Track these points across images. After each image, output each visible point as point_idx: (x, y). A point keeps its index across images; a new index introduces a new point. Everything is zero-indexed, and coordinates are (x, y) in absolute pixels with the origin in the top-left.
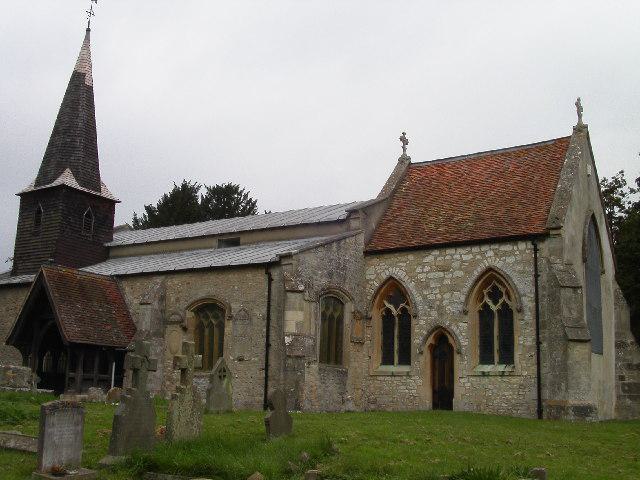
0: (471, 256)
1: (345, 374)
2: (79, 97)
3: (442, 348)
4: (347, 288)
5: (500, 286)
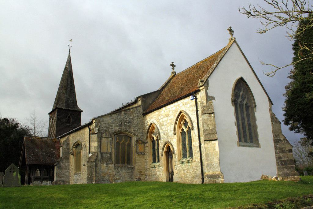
1: (134, 168)
2: (68, 75)
3: (169, 153)
4: (132, 130)
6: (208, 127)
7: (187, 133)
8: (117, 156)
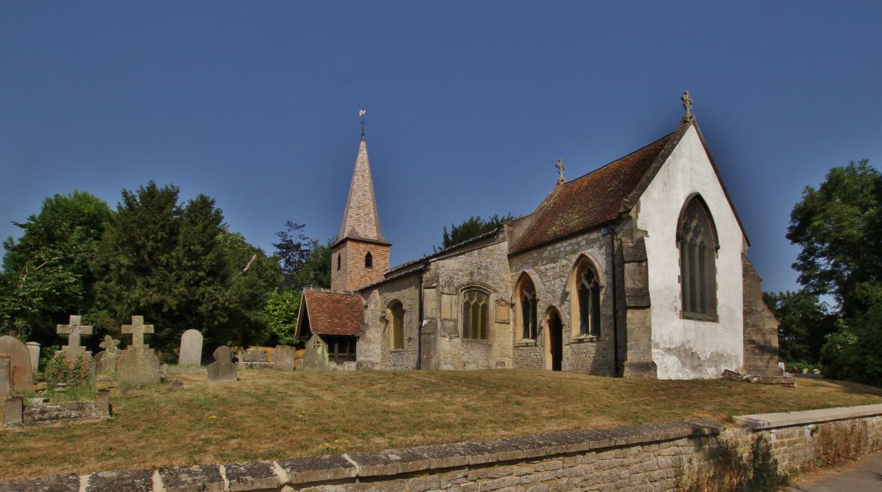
0: (571, 247)
1: (490, 346)
5: (591, 268)
6: (634, 283)
7: (590, 292)
8: (465, 325)
